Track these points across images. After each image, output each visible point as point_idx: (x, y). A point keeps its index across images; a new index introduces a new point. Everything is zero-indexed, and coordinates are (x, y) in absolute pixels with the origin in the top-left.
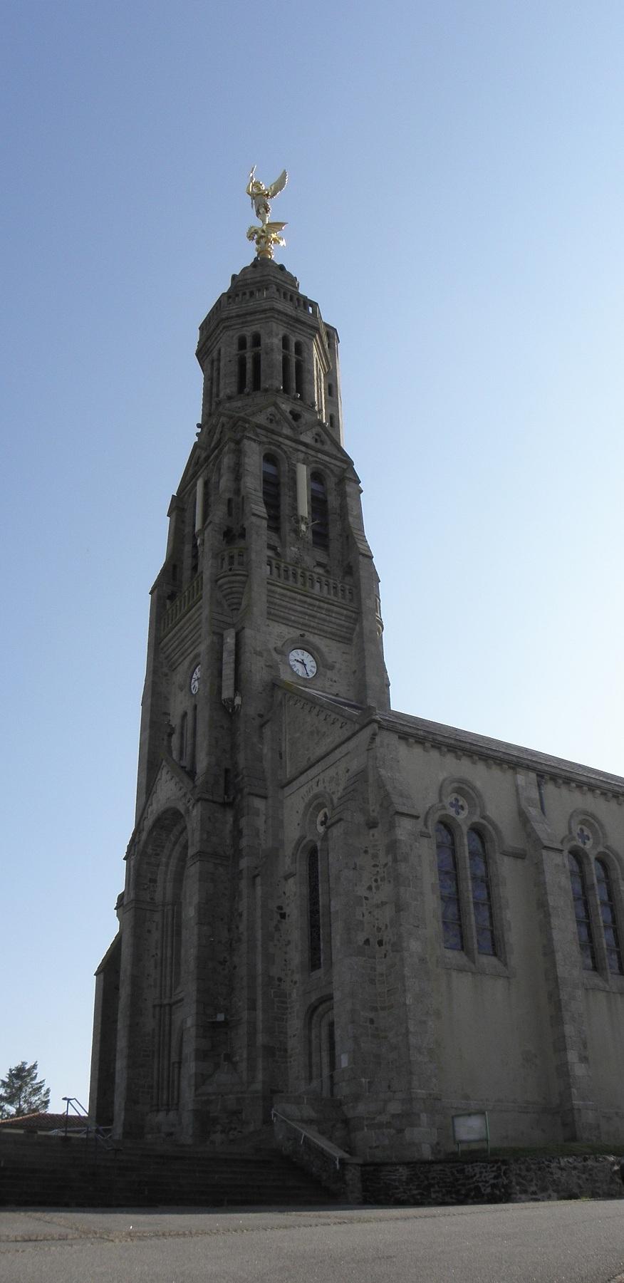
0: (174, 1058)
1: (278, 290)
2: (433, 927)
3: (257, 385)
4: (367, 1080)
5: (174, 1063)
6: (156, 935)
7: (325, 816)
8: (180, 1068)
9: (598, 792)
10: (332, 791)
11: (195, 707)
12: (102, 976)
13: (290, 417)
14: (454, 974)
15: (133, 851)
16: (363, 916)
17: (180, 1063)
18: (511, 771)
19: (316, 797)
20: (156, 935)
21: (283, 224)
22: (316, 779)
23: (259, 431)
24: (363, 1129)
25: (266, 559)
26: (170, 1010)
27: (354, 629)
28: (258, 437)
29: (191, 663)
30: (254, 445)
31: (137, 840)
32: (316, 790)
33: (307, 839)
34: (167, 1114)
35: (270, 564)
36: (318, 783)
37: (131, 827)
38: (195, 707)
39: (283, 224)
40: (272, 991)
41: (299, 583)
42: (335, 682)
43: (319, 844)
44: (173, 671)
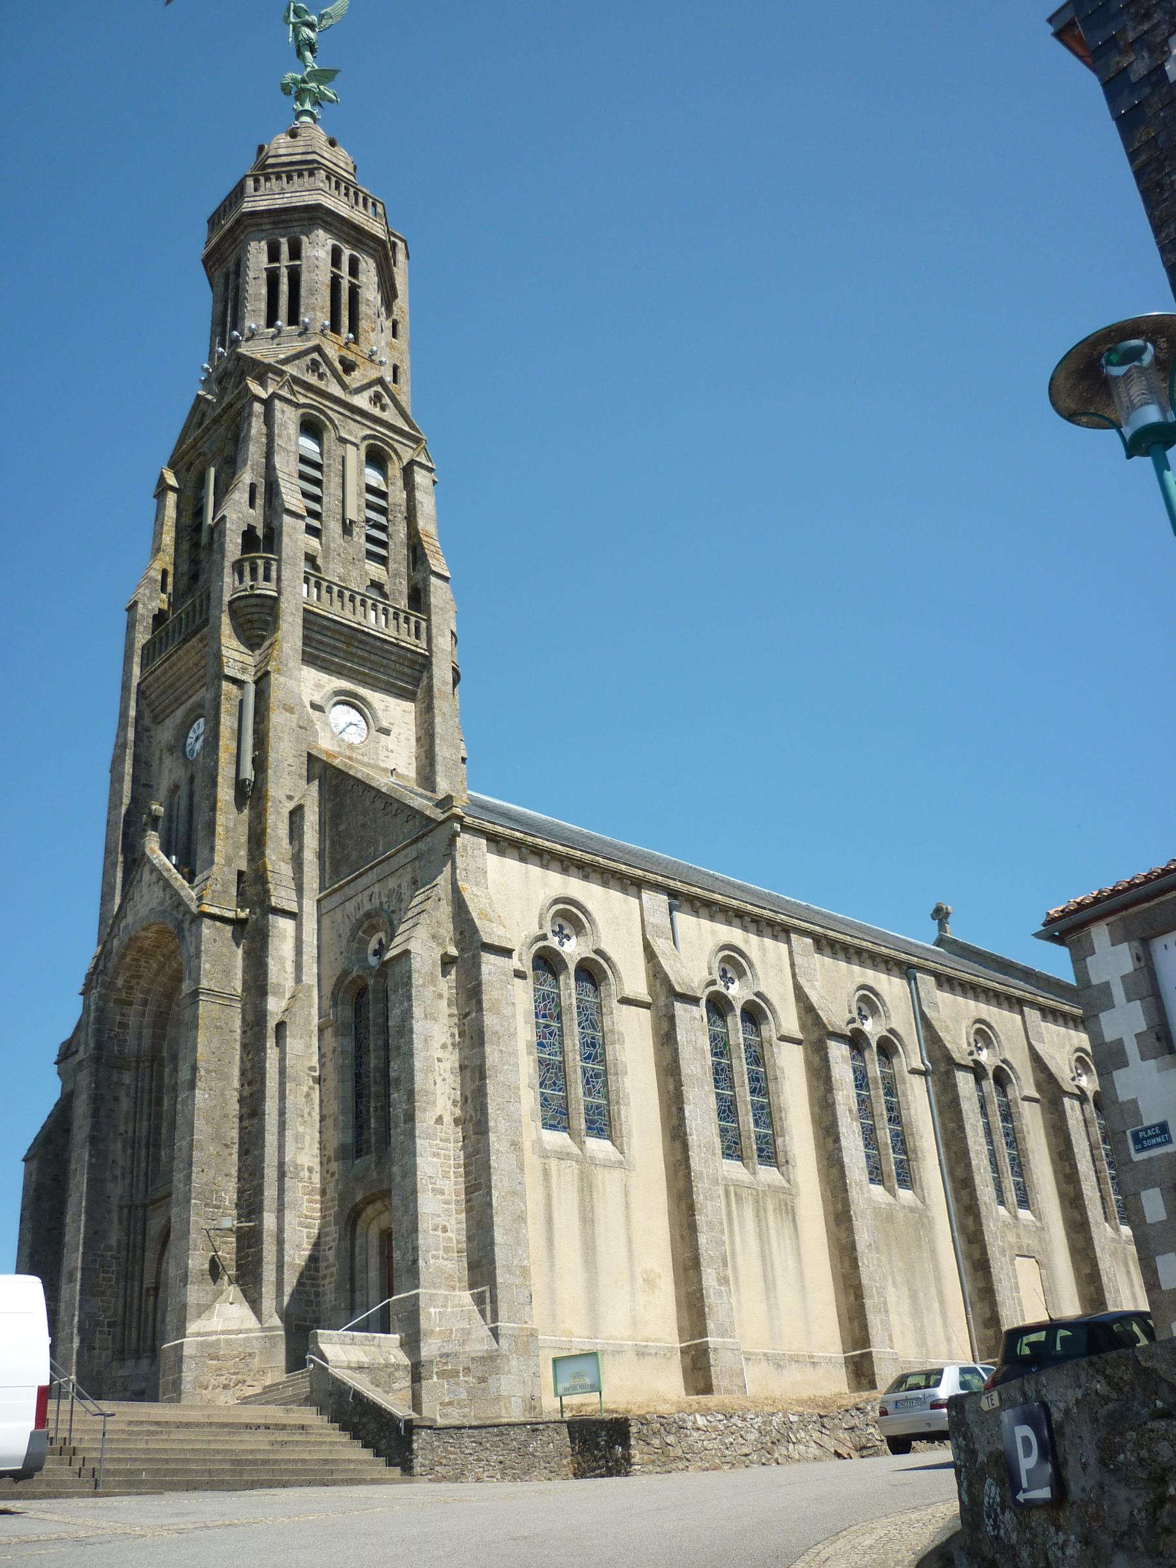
0: (149, 1281)
1: (328, 178)
2: (529, 1100)
3: (293, 319)
4: (438, 1310)
5: (147, 1290)
6: (125, 1104)
7: (380, 942)
8: (156, 1296)
9: (747, 918)
10: (391, 909)
11: (192, 779)
12: (34, 1164)
13: (339, 368)
14: (553, 1163)
15: (94, 982)
16: (435, 1084)
17: (156, 1289)
18: (635, 888)
19: (368, 915)
20: (125, 1104)
21: (336, 71)
22: (368, 892)
23: (296, 388)
24: (431, 1378)
25: (303, 575)
26: (145, 1214)
27: (419, 679)
28: (295, 395)
29: (187, 716)
30: (289, 410)
31: (101, 967)
32: (367, 907)
33: (354, 974)
34: (136, 1364)
35: (307, 581)
36: (371, 896)
37: (94, 949)
38: (192, 779)
39: (336, 71)
40: (300, 1185)
41: (347, 611)
42: (392, 751)
43: (371, 982)
44: (159, 723)
